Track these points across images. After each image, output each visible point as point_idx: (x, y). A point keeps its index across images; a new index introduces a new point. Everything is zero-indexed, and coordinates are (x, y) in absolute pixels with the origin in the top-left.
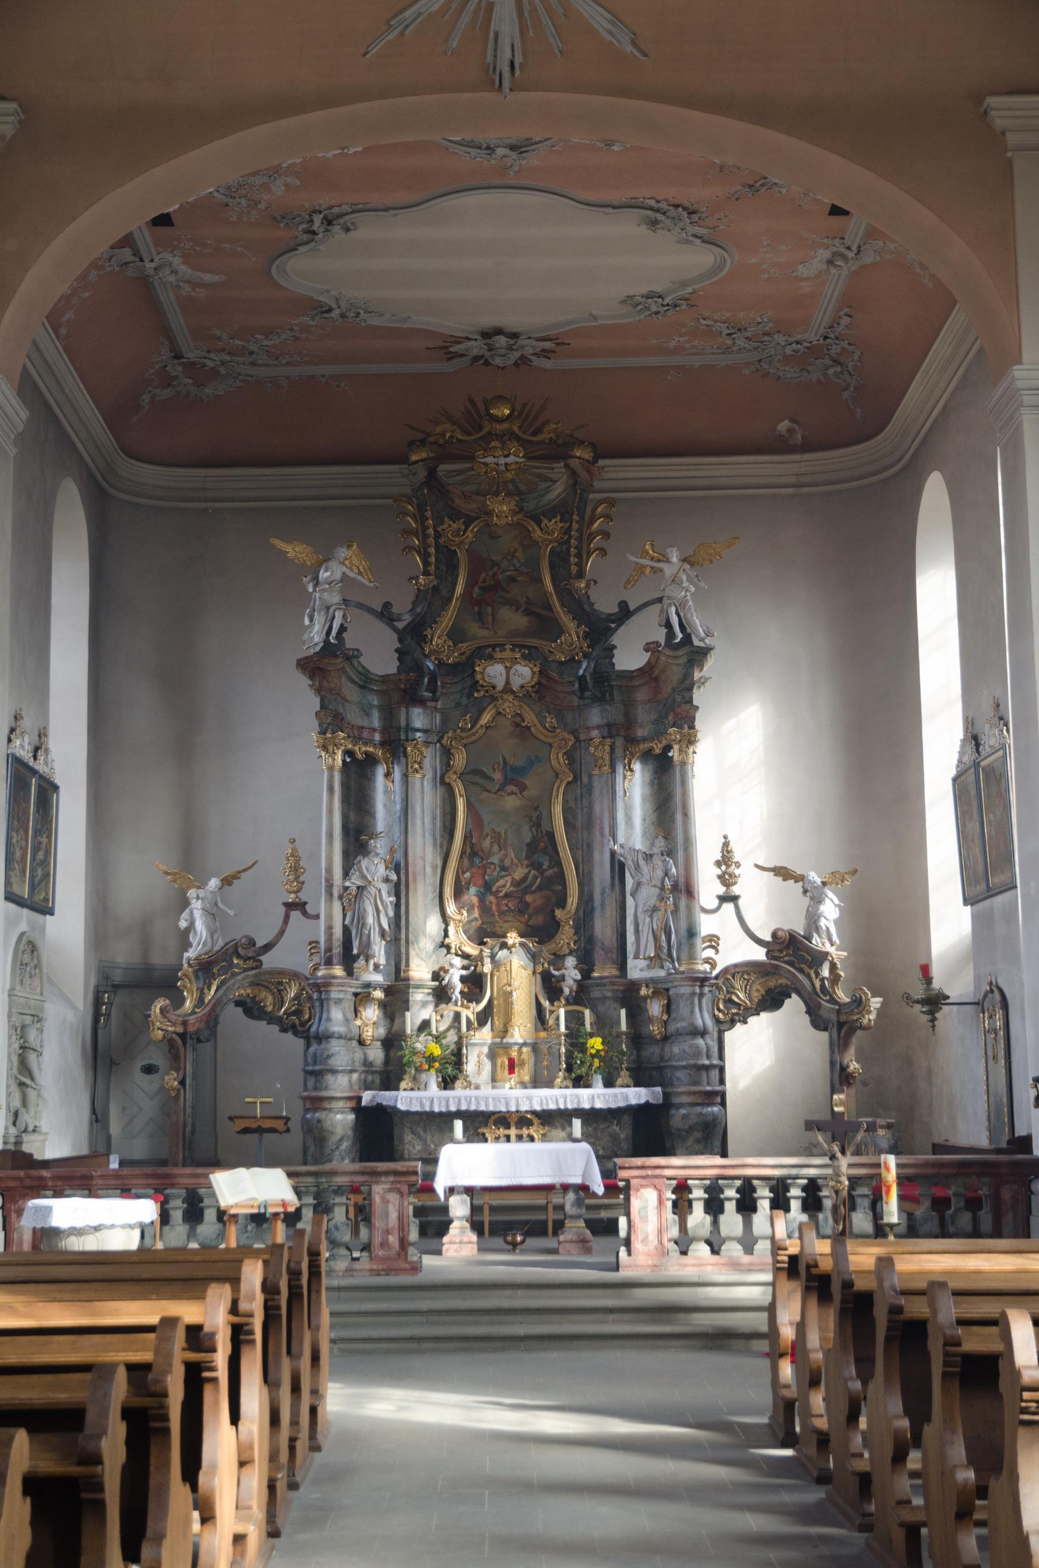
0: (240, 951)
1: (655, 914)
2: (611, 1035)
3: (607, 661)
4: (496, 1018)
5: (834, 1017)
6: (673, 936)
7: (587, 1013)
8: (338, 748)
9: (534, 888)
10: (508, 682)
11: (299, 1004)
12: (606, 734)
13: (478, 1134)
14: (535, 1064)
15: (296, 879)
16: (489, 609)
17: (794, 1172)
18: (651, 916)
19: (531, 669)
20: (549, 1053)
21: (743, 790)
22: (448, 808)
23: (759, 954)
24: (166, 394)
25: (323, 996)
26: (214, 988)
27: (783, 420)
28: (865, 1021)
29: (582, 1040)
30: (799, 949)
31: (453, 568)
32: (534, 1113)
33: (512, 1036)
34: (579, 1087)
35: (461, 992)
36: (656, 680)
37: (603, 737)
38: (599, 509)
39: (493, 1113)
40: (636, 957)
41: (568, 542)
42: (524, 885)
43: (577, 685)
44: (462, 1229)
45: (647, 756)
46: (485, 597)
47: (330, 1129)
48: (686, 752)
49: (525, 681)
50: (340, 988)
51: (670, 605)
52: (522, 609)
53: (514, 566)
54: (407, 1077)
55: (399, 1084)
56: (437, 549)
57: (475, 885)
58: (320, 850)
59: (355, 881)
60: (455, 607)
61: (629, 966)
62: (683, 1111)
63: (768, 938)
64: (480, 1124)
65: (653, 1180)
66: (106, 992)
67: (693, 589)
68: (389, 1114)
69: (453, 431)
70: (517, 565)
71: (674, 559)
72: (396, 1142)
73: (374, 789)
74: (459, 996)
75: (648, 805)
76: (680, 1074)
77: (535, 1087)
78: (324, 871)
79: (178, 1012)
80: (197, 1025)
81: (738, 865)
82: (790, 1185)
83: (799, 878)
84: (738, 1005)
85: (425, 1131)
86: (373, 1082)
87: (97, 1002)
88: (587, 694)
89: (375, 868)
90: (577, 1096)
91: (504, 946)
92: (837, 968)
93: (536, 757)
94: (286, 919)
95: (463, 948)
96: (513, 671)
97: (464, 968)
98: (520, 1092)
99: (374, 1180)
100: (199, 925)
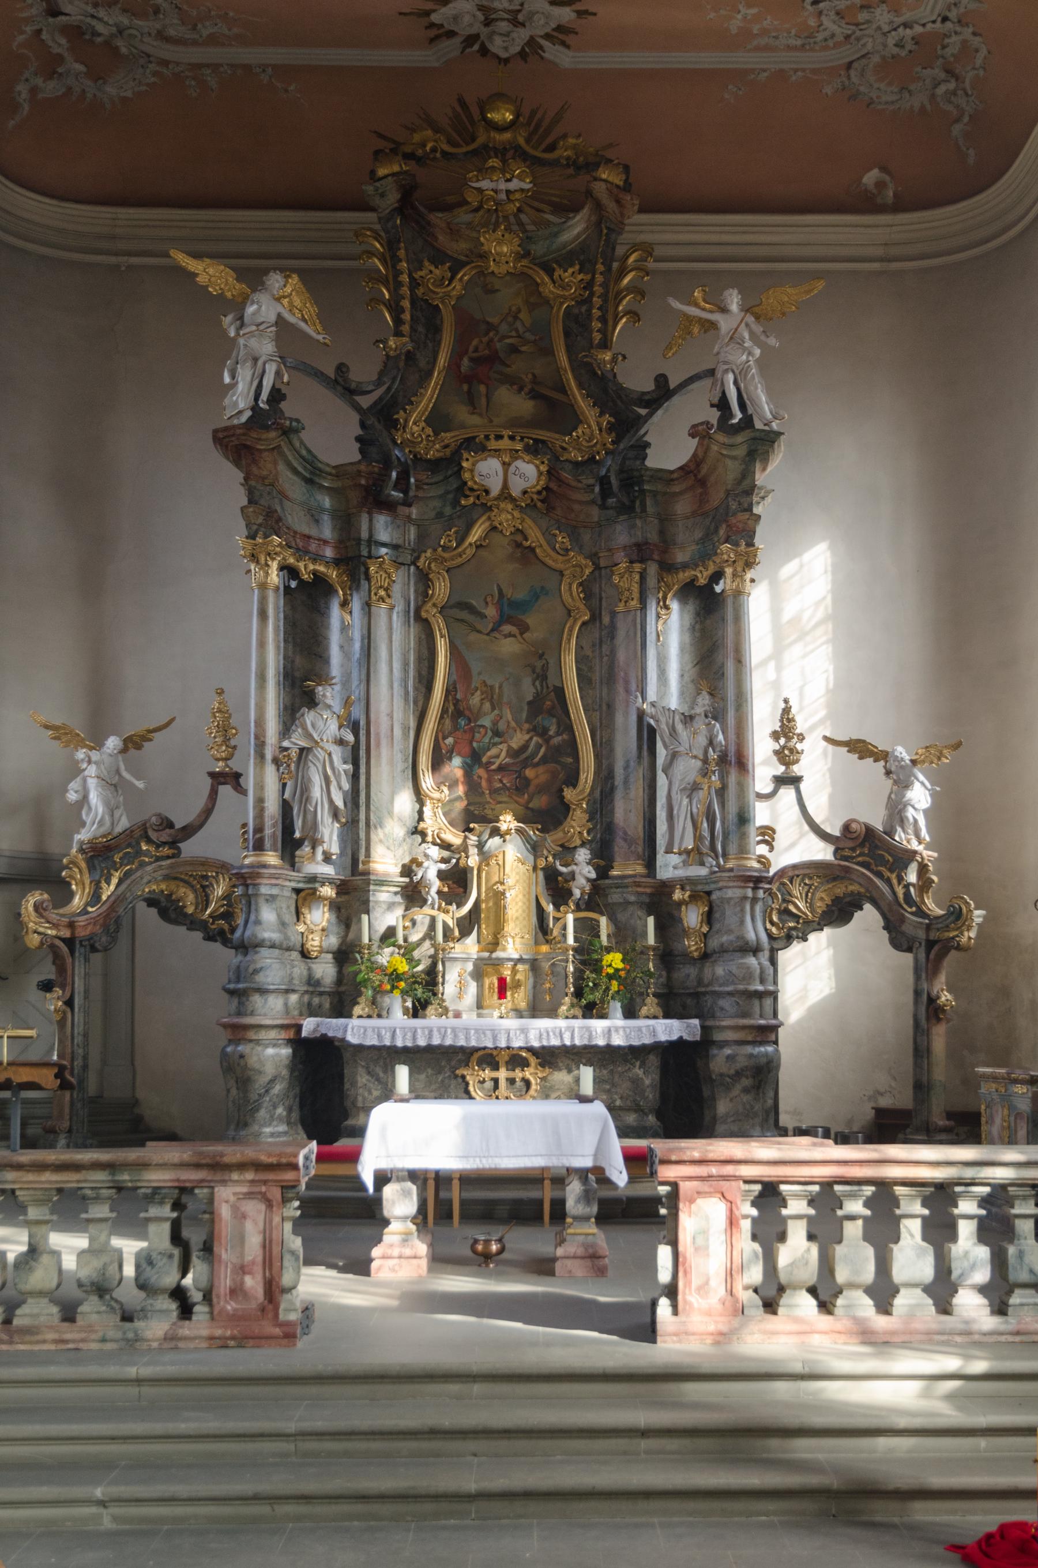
1: (694, 794)
2: (634, 950)
3: (638, 462)
4: (483, 926)
5: (921, 934)
6: (718, 824)
7: (603, 921)
8: (273, 559)
9: (536, 760)
10: (505, 485)
11: (229, 905)
12: (635, 557)
13: (456, 1076)
14: (534, 987)
15: (226, 741)
16: (482, 388)
17: (969, 1173)
18: (690, 797)
19: (537, 467)
20: (552, 973)
21: (810, 641)
22: (425, 652)
23: (822, 852)
24: (51, 88)
25: (250, 892)
26: (115, 881)
27: (870, 169)
28: (964, 940)
29: (595, 956)
30: (877, 847)
31: (434, 329)
32: (530, 1050)
33: (504, 949)
34: (591, 1017)
35: (439, 892)
36: (702, 482)
37: (631, 562)
38: (631, 259)
39: (477, 1049)
40: (669, 851)
41: (588, 301)
42: (524, 756)
43: (597, 489)
44: (406, 1238)
45: (689, 591)
46: (480, 370)
47: (257, 1066)
50: (274, 881)
51: (726, 371)
52: (526, 390)
53: (517, 330)
54: (362, 1000)
55: (352, 1009)
56: (413, 303)
57: (459, 754)
59: (297, 740)
61: (658, 863)
62: (728, 1051)
64: (445, 1069)
67: (757, 352)
68: (338, 1049)
70: (521, 330)
71: (734, 307)
72: (347, 1086)
73: (327, 627)
74: (436, 897)
75: (687, 657)
76: (725, 1003)
78: (253, 724)
79: (61, 911)
80: (90, 928)
82: (959, 1195)
86: (320, 1006)
88: (611, 501)
89: (324, 725)
90: (588, 1029)
91: (496, 832)
92: (928, 871)
93: (543, 588)
94: (213, 794)
95: (443, 836)
96: (512, 469)
97: (444, 861)
98: (512, 1023)
99: (218, 1176)
100: (94, 797)
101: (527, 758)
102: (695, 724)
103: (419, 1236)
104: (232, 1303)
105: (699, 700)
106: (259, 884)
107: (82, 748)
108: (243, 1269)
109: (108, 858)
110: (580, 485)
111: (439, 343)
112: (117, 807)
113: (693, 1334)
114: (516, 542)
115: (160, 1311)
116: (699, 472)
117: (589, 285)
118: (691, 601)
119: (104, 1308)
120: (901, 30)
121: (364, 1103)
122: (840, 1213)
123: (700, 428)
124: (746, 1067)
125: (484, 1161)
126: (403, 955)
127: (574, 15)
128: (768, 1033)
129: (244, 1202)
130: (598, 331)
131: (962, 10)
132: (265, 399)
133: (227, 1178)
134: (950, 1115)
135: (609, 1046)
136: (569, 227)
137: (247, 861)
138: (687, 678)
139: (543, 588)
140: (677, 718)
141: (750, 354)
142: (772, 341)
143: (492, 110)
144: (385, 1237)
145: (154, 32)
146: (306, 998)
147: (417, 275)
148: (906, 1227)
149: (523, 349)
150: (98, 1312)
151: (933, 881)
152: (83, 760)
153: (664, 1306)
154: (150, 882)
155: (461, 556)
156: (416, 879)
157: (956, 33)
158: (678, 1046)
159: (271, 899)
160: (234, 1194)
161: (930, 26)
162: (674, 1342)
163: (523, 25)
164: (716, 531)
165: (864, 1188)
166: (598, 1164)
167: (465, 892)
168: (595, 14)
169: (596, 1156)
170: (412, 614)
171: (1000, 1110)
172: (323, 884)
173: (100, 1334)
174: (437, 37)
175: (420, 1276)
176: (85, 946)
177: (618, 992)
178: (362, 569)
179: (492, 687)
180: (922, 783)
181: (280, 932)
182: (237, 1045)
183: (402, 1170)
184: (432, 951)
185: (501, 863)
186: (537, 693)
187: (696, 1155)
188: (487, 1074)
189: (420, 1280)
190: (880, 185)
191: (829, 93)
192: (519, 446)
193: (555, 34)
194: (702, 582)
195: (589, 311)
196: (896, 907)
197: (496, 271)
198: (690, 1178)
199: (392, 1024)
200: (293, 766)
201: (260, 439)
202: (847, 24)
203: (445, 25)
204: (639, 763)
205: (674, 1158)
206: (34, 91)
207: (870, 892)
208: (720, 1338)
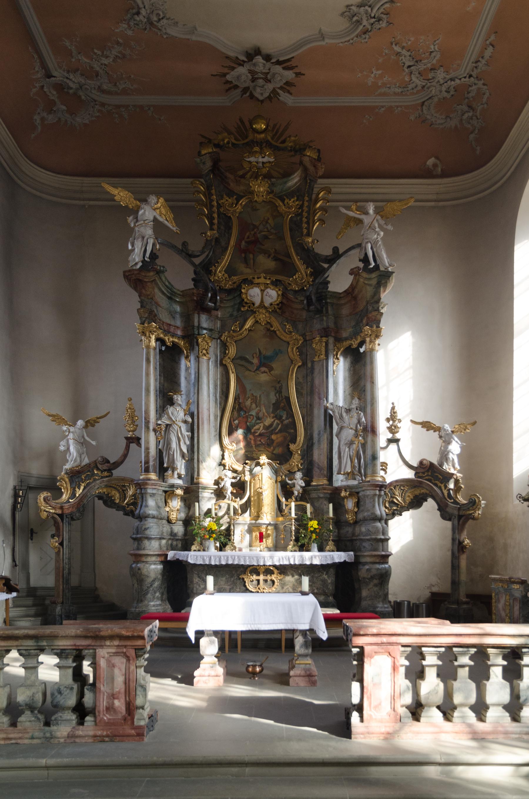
0: (100, 466)
2: (323, 519)
4: (252, 508)
5: (456, 512)
6: (362, 460)
8: (153, 334)
10: (262, 301)
11: (135, 499)
13: (240, 579)
14: (276, 537)
15: (133, 422)
16: (251, 256)
18: (349, 447)
19: (277, 292)
20: (285, 530)
23: (409, 474)
24: (51, 119)
25: (143, 492)
26: (82, 488)
28: (476, 515)
30: (435, 472)
31: (229, 228)
32: (275, 566)
34: (303, 551)
35: (232, 493)
36: (355, 298)
37: (321, 337)
38: (320, 195)
39: (249, 566)
40: (339, 473)
41: (301, 215)
43: (305, 302)
46: (248, 250)
47: (146, 573)
48: (374, 342)
49: (273, 300)
50: (154, 487)
51: (367, 243)
52: (272, 256)
53: (267, 228)
54: (196, 543)
56: (218, 216)
57: (241, 428)
58: (142, 400)
59: (165, 421)
60: (230, 253)
62: (367, 567)
64: (234, 577)
65: (386, 647)
66: (21, 490)
69: (229, 138)
70: (269, 228)
71: (371, 212)
72: (189, 583)
73: (179, 369)
74: (230, 495)
75: (347, 383)
76: (366, 544)
77: (276, 550)
78: (143, 413)
79: (57, 501)
80: (70, 509)
83: (437, 429)
84: (397, 505)
86: (177, 545)
87: (16, 496)
88: (312, 308)
89: (177, 413)
90: (301, 556)
91: (258, 464)
94: (128, 448)
95: (233, 466)
96: (265, 293)
97: (234, 478)
98: (266, 554)
99: (98, 643)
100: (72, 449)
101: (272, 430)
102: (351, 413)
103: (219, 664)
104: (107, 715)
105: (354, 401)
107: (65, 425)
108: (113, 696)
109: (79, 477)
110: (297, 301)
111: (231, 233)
112: (83, 453)
113: (373, 733)
114: (267, 328)
115: (65, 720)
116: (353, 293)
118: (349, 358)
119: (33, 719)
120: (449, 82)
122: (456, 663)
123: (355, 270)
125: (252, 626)
126: (215, 522)
127: (294, 75)
128: (385, 558)
129: (114, 657)
130: (305, 228)
131: (479, 70)
132: (148, 256)
133: (103, 644)
134: (468, 596)
137: (141, 477)
138: (347, 393)
140: (343, 410)
141: (378, 234)
142: (390, 227)
143: (255, 123)
144: (201, 665)
145: (97, 87)
146: (170, 542)
147: (221, 202)
148: (493, 671)
149: (270, 237)
150: (30, 721)
151: (462, 487)
152: (66, 431)
153: (355, 716)
154: (98, 488)
155: (241, 335)
156: (221, 486)
157: (475, 84)
158: (343, 565)
159: (152, 495)
160: (108, 653)
161: (463, 79)
162: (361, 738)
163: (270, 82)
164: (362, 321)
165: (471, 649)
166: (312, 628)
167: (244, 492)
168: (304, 75)
169: (310, 625)
170: (218, 362)
171: (504, 596)
172: (177, 489)
173: (30, 734)
174: (229, 89)
175: (219, 686)
176: (68, 518)
177: (315, 539)
178: (195, 340)
179: (256, 397)
180: (457, 442)
181: (157, 511)
182: (137, 564)
183: (210, 631)
184: (229, 520)
185: (260, 479)
187: (375, 631)
188: (255, 577)
189: (219, 689)
190: (435, 165)
191: (413, 120)
193: (285, 86)
194: (355, 346)
195: (301, 220)
196: (444, 500)
197: (258, 200)
198: (371, 644)
199: (211, 554)
200: (163, 432)
201: (146, 276)
202: (423, 79)
203: (233, 81)
204: (325, 432)
205: (362, 633)
206: (43, 119)
207: (431, 493)
208: (388, 736)
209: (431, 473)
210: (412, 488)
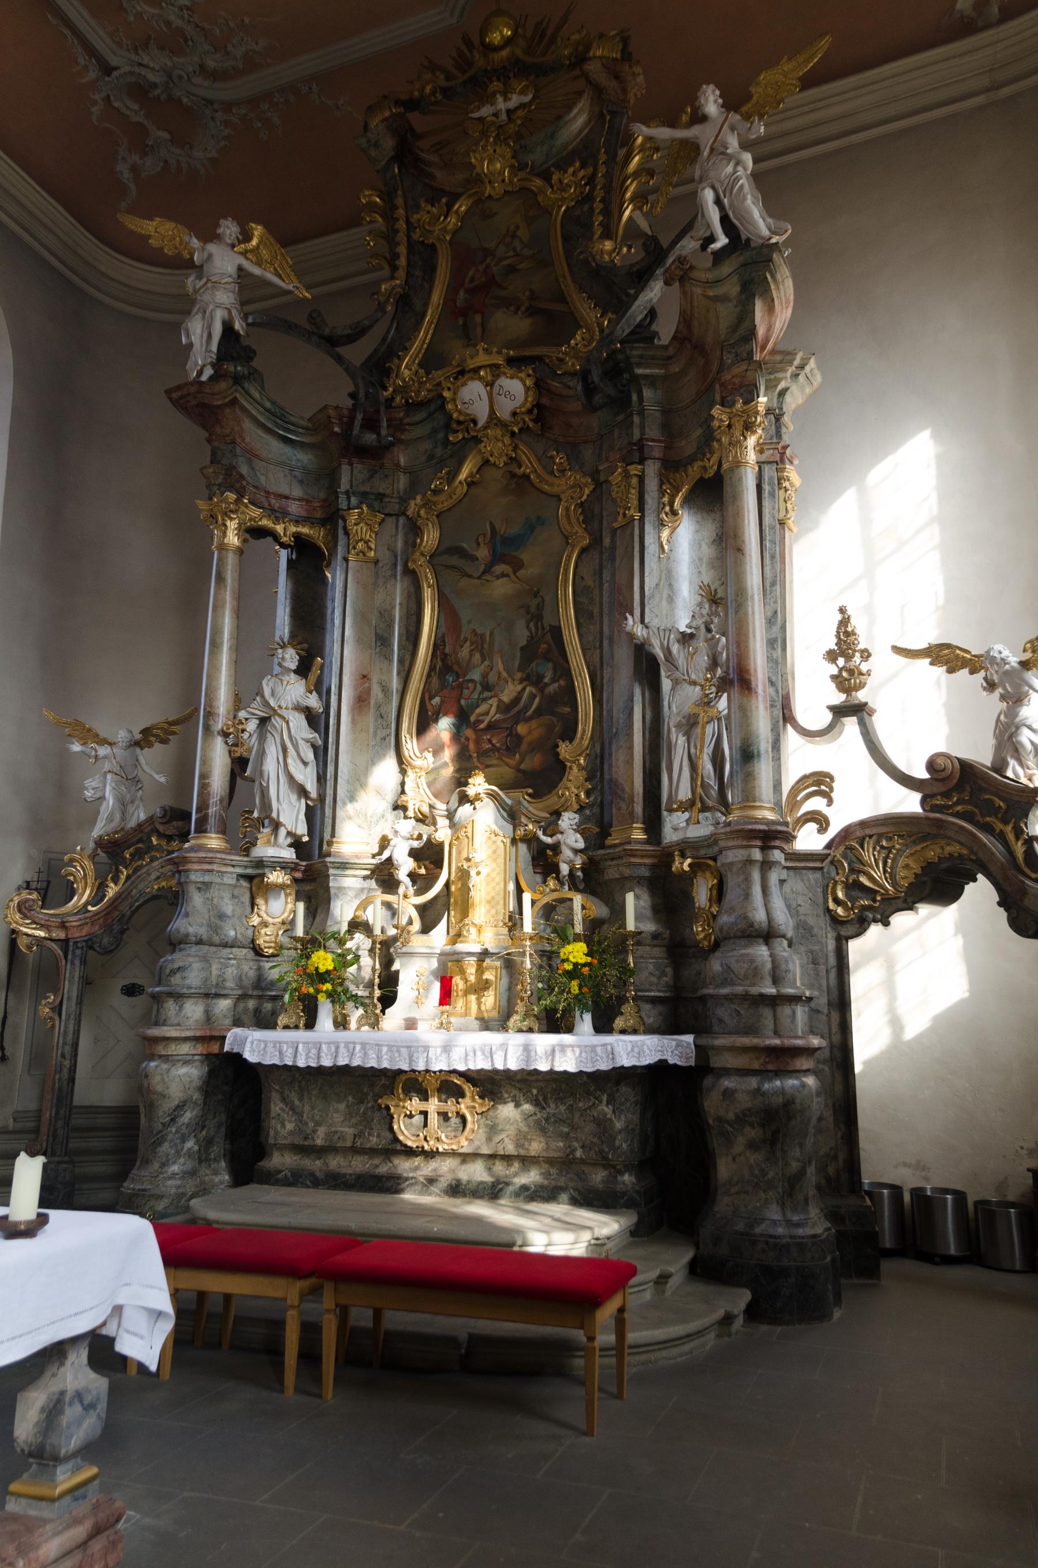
4: (452, 913)
9: (530, 713)
14: (510, 989)
16: (478, 318)
22: (414, 606)
23: (911, 803)
25: (183, 880)
31: (431, 270)
41: (589, 198)
42: (516, 709)
47: (159, 1088)
50: (206, 867)
52: (523, 309)
53: (514, 249)
57: (445, 714)
62: (727, 1083)
63: (921, 773)
72: (263, 1116)
76: (723, 1012)
81: (866, 655)
85: (301, 1099)
88: (598, 399)
93: (539, 518)
101: (519, 712)
106: (189, 870)
114: (510, 472)
117: (591, 180)
121: (276, 1139)
124: (749, 1110)
135: (551, 1072)
136: (567, 123)
139: (539, 518)
149: (521, 266)
158: (660, 1069)
179: (482, 636)
185: (470, 835)
186: (532, 637)
188: (415, 1104)
192: (500, 361)
195: (592, 210)
196: (1012, 872)
201: (214, 394)
206: (135, 169)
207: (975, 854)
209: (971, 795)
210: (914, 842)
